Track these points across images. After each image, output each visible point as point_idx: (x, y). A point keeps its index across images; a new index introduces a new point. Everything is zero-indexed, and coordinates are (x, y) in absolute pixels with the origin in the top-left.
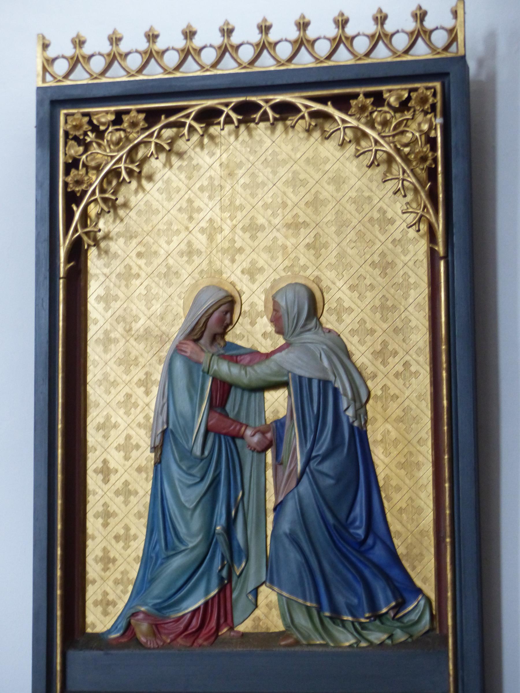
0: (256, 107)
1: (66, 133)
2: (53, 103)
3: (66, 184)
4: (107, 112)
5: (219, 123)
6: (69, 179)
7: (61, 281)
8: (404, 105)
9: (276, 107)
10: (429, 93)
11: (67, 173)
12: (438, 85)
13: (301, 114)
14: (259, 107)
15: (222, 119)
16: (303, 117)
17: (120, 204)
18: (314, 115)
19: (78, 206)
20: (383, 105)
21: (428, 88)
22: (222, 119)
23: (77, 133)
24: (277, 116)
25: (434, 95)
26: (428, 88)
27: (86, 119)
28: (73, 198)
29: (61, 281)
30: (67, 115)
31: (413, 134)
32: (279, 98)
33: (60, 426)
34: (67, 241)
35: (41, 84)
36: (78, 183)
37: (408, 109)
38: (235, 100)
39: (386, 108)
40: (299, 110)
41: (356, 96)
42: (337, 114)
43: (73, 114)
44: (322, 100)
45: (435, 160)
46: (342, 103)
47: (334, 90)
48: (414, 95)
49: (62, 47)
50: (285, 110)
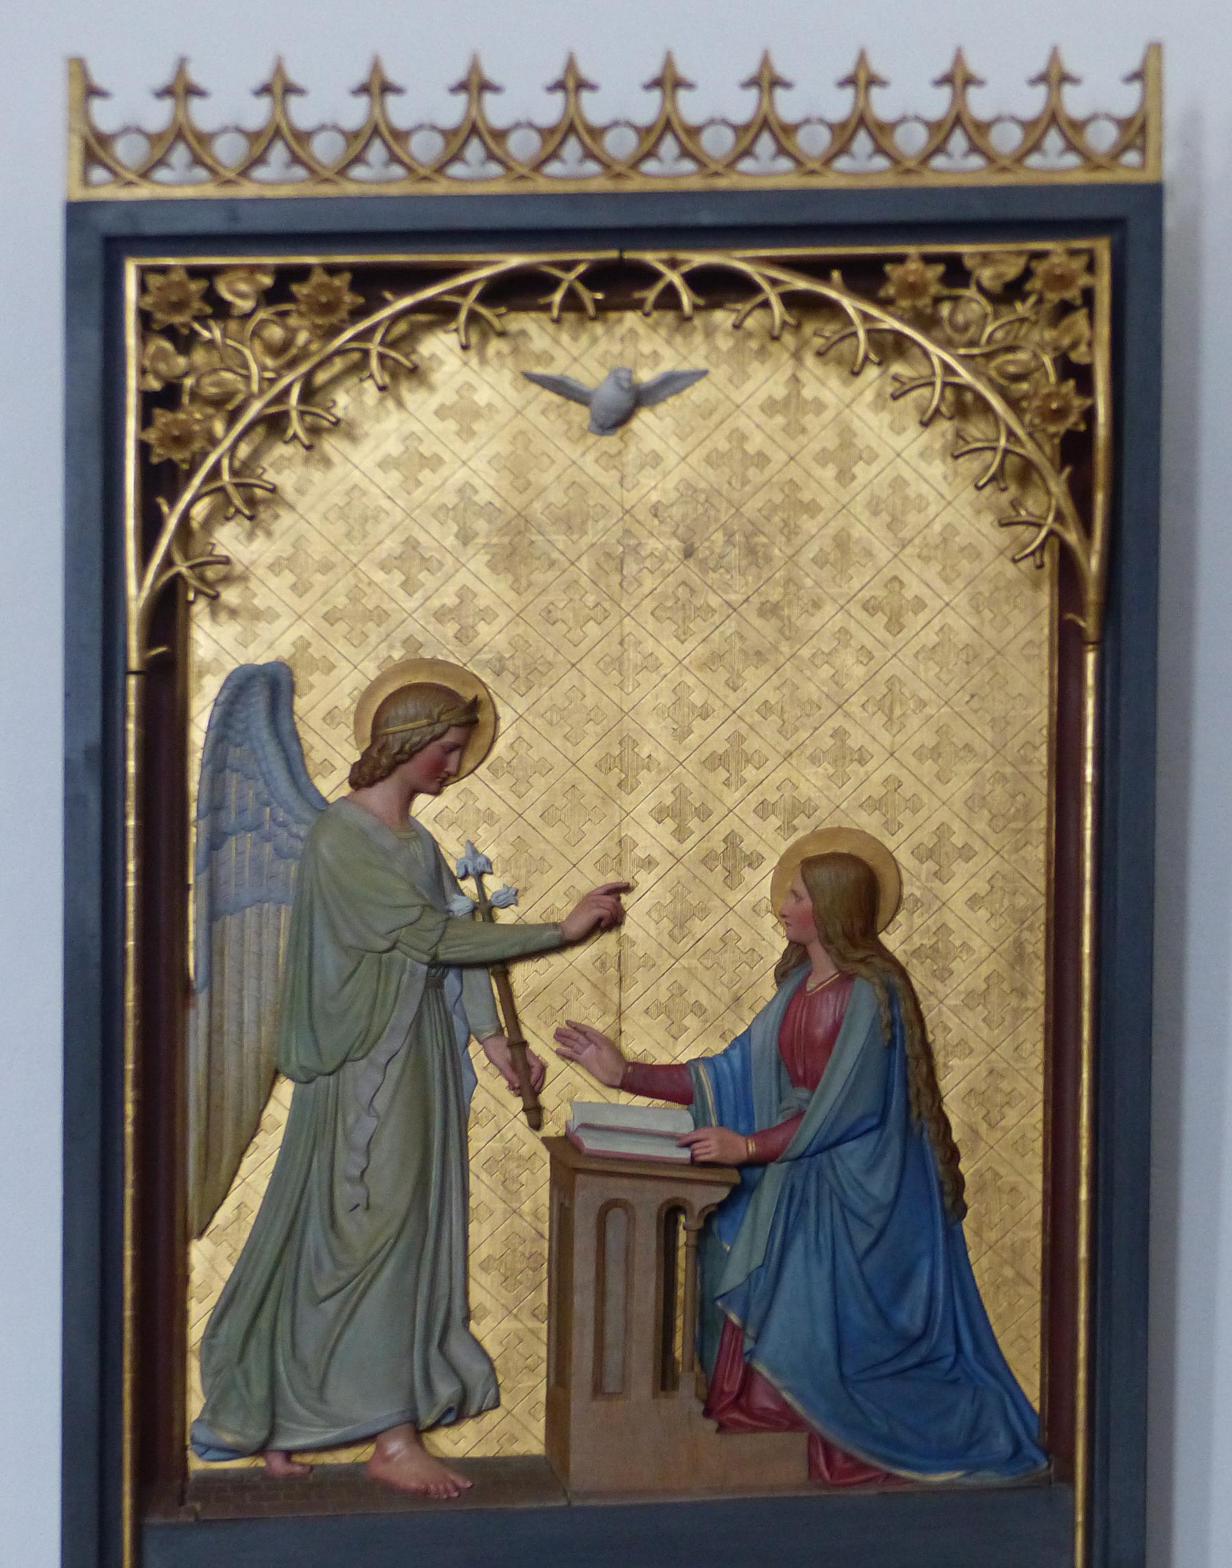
0: (649, 276)
1: (145, 318)
2: (100, 245)
3: (144, 449)
4: (254, 269)
5: (547, 308)
6: (152, 436)
7: (132, 682)
8: (1012, 291)
9: (700, 280)
10: (1078, 264)
11: (146, 421)
12: (1103, 248)
13: (760, 298)
14: (656, 276)
15: (557, 297)
16: (766, 305)
17: (432, 1450)
18: (792, 300)
19: (172, 503)
20: (966, 285)
21: (1073, 253)
22: (557, 297)
23: (178, 319)
24: (791, 320)
25: (1091, 268)
26: (1073, 253)
27: (196, 286)
28: (161, 480)
29: (132, 682)
30: (143, 272)
31: (1035, 356)
32: (699, 259)
33: (130, 1066)
34: (145, 593)
35: (79, 194)
36: (181, 441)
37: (1024, 297)
38: (586, 257)
39: (971, 292)
40: (754, 289)
41: (900, 259)
42: (849, 304)
43: (163, 270)
44: (817, 269)
45: (1089, 415)
46: (865, 277)
47: (838, 243)
48: (1041, 267)
49: (132, 107)
50: (718, 287)
